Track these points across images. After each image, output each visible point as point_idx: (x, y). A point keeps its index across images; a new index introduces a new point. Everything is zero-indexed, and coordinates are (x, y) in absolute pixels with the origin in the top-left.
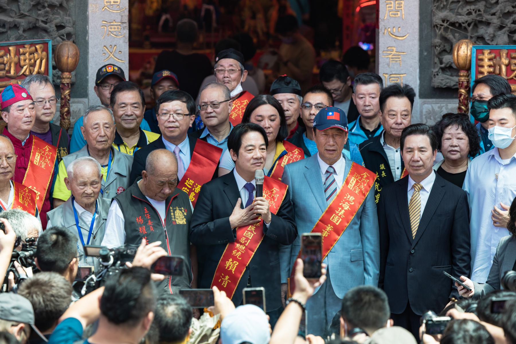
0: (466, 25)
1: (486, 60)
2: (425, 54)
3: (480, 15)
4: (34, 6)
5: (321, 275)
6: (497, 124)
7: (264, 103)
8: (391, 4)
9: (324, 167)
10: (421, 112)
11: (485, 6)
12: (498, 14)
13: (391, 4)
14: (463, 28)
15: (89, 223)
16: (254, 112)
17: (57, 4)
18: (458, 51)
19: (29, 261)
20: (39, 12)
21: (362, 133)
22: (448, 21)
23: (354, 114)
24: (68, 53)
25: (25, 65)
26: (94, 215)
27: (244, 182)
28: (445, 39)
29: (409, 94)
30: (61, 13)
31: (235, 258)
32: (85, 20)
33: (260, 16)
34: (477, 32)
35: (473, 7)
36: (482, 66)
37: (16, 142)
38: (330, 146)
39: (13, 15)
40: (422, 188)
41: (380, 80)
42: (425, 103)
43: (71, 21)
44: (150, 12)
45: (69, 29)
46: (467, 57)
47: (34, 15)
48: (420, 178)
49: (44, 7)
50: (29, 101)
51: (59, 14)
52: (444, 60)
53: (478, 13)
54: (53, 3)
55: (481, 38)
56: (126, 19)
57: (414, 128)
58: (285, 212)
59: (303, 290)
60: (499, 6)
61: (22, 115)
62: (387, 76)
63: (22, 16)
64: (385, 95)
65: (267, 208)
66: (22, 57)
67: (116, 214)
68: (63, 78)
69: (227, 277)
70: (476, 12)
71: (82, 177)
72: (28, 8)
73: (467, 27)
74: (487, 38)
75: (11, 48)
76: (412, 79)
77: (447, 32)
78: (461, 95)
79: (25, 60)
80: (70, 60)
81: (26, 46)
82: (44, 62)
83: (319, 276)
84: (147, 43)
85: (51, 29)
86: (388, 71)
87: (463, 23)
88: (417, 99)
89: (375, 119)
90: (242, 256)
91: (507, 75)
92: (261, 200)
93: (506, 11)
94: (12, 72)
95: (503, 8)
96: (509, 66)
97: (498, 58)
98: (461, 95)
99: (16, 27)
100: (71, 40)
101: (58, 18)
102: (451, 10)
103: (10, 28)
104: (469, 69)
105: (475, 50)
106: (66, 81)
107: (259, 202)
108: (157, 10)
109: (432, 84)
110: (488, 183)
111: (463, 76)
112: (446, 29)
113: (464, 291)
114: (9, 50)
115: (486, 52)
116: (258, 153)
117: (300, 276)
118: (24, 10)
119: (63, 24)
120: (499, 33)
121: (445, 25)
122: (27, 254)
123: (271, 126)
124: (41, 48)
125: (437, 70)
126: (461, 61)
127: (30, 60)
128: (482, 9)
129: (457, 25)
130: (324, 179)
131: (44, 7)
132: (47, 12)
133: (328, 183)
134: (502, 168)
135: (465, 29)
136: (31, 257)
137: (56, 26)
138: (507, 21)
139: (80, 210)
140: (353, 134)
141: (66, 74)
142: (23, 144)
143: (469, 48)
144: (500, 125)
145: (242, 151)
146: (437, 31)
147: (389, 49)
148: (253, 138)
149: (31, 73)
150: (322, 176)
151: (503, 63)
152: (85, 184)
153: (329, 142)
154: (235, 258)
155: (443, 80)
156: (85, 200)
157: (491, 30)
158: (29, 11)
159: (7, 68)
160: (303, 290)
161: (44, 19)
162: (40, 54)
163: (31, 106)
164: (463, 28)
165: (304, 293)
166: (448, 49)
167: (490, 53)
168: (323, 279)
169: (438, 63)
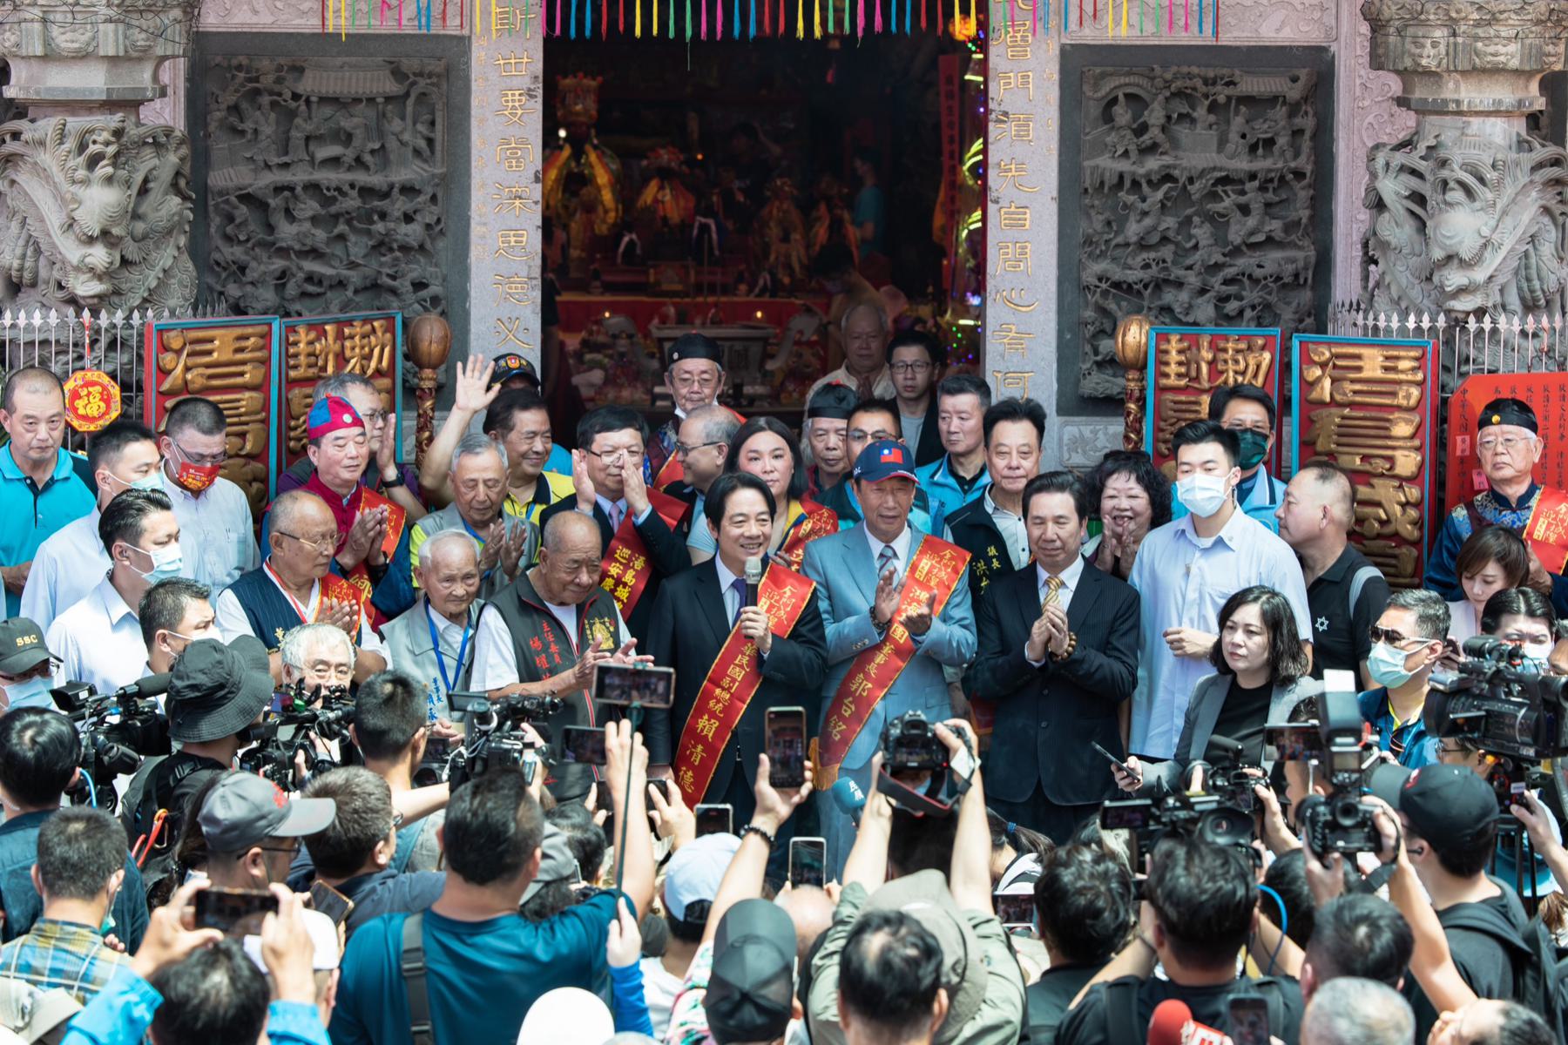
0: (1140, 286)
1: (1174, 353)
3: (1166, 269)
4: (373, 247)
5: (803, 781)
7: (762, 429)
9: (877, 546)
10: (1060, 439)
11: (1175, 253)
12: (1197, 267)
15: (458, 647)
17: (415, 244)
18: (1124, 335)
19: (336, 727)
21: (951, 481)
23: (932, 448)
24: (431, 333)
26: (466, 631)
28: (1103, 311)
29: (1035, 415)
31: (712, 715)
32: (464, 273)
33: (796, 236)
34: (1160, 298)
35: (1152, 255)
36: (1167, 364)
37: (331, 498)
39: (337, 264)
40: (1063, 584)
41: (983, 389)
42: (1066, 424)
44: (602, 229)
45: (435, 289)
47: (374, 265)
48: (1056, 568)
49: (391, 250)
50: (357, 430)
51: (418, 262)
52: (1101, 349)
55: (1167, 309)
56: (537, 272)
57: (1045, 482)
58: (804, 630)
59: (769, 810)
61: (342, 454)
63: (353, 265)
64: (994, 416)
66: (348, 344)
69: (700, 748)
71: (447, 566)
72: (363, 252)
74: (1177, 310)
75: (328, 327)
76: (1043, 388)
78: (1129, 414)
79: (353, 349)
80: (434, 347)
82: (387, 350)
83: (800, 784)
84: (597, 283)
85: (404, 290)
88: (1053, 421)
89: (973, 457)
90: (725, 710)
91: (1210, 380)
94: (330, 369)
98: (1129, 414)
99: (341, 284)
100: (439, 309)
101: (415, 271)
102: (1114, 259)
103: (331, 287)
104: (1144, 367)
106: (427, 385)
107: (751, 615)
108: (615, 225)
109: (1081, 391)
110: (1171, 576)
112: (1105, 294)
113: (1127, 781)
115: (1174, 339)
116: (753, 529)
117: (763, 786)
120: (1200, 300)
121: (1104, 286)
122: (331, 715)
125: (1088, 365)
126: (1130, 354)
127: (362, 348)
130: (877, 565)
131: (391, 250)
132: (396, 259)
134: (1198, 554)
136: (338, 720)
137: (413, 284)
138: (1213, 280)
139: (441, 623)
140: (937, 484)
141: (428, 372)
142: (345, 502)
145: (725, 522)
148: (745, 501)
149: (364, 371)
152: (451, 579)
154: (712, 715)
155: (1098, 383)
156: (453, 608)
157: (1184, 296)
158: (365, 256)
159: (320, 363)
160: (769, 810)
162: (381, 336)
165: (770, 816)
166: (1109, 330)
167: (1180, 340)
168: (806, 789)
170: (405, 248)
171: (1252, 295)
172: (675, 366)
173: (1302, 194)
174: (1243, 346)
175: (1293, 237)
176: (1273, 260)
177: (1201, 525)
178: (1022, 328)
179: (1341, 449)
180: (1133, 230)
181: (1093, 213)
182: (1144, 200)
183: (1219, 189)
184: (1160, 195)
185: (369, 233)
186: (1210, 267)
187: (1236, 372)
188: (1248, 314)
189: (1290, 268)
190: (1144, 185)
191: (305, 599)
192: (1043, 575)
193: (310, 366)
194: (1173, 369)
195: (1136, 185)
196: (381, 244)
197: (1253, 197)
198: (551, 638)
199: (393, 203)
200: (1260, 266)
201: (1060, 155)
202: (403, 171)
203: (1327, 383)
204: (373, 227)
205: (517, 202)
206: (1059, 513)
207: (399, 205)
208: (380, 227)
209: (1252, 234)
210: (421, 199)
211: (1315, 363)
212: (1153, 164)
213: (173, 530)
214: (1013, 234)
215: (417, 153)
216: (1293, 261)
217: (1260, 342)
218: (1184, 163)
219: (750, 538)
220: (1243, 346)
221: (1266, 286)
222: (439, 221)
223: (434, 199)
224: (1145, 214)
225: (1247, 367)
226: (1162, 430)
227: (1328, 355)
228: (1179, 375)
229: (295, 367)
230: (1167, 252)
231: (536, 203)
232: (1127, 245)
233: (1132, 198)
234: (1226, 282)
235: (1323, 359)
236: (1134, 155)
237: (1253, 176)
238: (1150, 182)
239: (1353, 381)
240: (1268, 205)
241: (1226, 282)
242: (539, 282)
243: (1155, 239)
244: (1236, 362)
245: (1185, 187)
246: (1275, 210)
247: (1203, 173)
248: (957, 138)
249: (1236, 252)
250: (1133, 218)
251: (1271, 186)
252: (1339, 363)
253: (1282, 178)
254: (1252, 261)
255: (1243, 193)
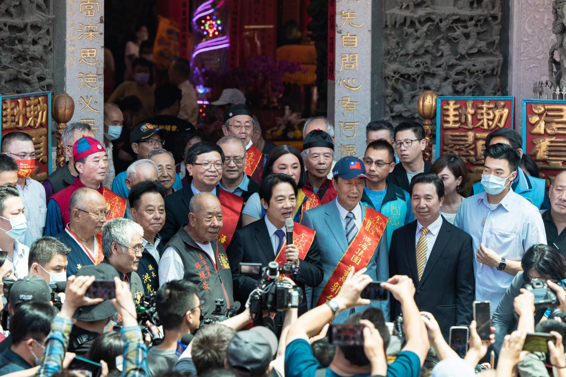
2: (377, 103)
3: (426, 67)
4: (15, 58)
6: (493, 173)
7: (286, 152)
8: (346, 57)
9: (344, 213)
12: (444, 66)
13: (346, 57)
14: (411, 79)
16: (277, 161)
18: (423, 101)
20: (21, 65)
22: (399, 73)
25: (30, 117)
27: (275, 229)
30: (42, 65)
32: (63, 72)
34: (423, 83)
35: (420, 60)
36: (448, 116)
38: (354, 193)
43: (50, 73)
45: (48, 81)
46: (432, 107)
52: (395, 109)
53: (425, 65)
54: (35, 56)
56: (101, 71)
57: (421, 177)
58: (311, 257)
60: (444, 59)
61: (98, 166)
62: (342, 124)
65: (298, 254)
67: (175, 261)
68: (60, 129)
70: (423, 65)
72: (9, 61)
73: (416, 78)
77: (397, 83)
79: (30, 112)
81: (31, 98)
82: (45, 113)
85: (34, 81)
86: (343, 119)
87: (413, 75)
91: (473, 124)
92: (293, 247)
93: (450, 63)
94: (21, 124)
95: (448, 61)
96: (475, 116)
97: (464, 108)
101: (38, 71)
105: (439, 100)
107: (291, 249)
111: (428, 125)
112: (397, 80)
114: (18, 103)
115: (451, 103)
116: (288, 203)
118: (5, 62)
119: (43, 76)
120: (444, 84)
121: (397, 76)
123: (294, 173)
124: (43, 100)
126: (427, 111)
127: (34, 112)
128: (429, 62)
129: (406, 77)
130: (344, 225)
131: (25, 59)
132: (29, 64)
133: (349, 228)
135: (414, 80)
137: (38, 78)
138: (451, 73)
143: (434, 99)
144: (496, 174)
145: (272, 201)
146: (389, 82)
147: (344, 99)
150: (342, 221)
151: (469, 113)
153: (353, 190)
157: (436, 81)
161: (26, 71)
163: (105, 158)
164: (411, 79)
167: (455, 104)
169: (389, 112)
170: (33, 59)
171: (470, 81)
172: (230, 121)
173: (497, 28)
174: (491, 106)
175: (491, 50)
176: (481, 62)
177: (494, 199)
178: (353, 99)
179: (550, 158)
180: (411, 47)
181: (390, 38)
182: (416, 31)
183: (454, 25)
184: (425, 28)
185: (12, 50)
186: (449, 66)
187: (488, 120)
188: (468, 90)
189: (490, 66)
190: (417, 24)
191: (91, 246)
192: (420, 226)
193: (12, 122)
194: (451, 119)
195: (412, 23)
196: (20, 56)
197: (471, 29)
198: (205, 263)
199: (27, 34)
200: (474, 65)
201: (373, 8)
202: (31, 17)
203: (542, 124)
204: (15, 47)
205: (91, 33)
206: (428, 193)
207: (31, 35)
208: (19, 47)
209: (471, 48)
210: (42, 31)
211: (535, 114)
212: (421, 12)
213: (21, 208)
214: (348, 49)
215: (39, 7)
216: (492, 62)
217: (502, 104)
218: (438, 11)
219: (287, 208)
220: (491, 106)
221: (477, 76)
222: (50, 43)
223: (48, 32)
224: (418, 38)
225: (495, 116)
226: (446, 151)
227: (543, 109)
228: (455, 122)
229: (6, 122)
230: (428, 58)
231: (101, 34)
232: (407, 55)
233: (411, 30)
234: (458, 74)
235: (540, 111)
236: (412, 7)
237: (471, 19)
238: (420, 22)
239: (557, 123)
240: (478, 33)
241: (458, 74)
242: (102, 77)
243: (422, 51)
244: (489, 114)
245: (438, 23)
246: (481, 36)
247: (449, 16)
248: (188, 4)
249: (462, 57)
250: (411, 41)
251: (479, 23)
252: (549, 113)
253: (486, 20)
254: (471, 63)
255: (466, 27)
